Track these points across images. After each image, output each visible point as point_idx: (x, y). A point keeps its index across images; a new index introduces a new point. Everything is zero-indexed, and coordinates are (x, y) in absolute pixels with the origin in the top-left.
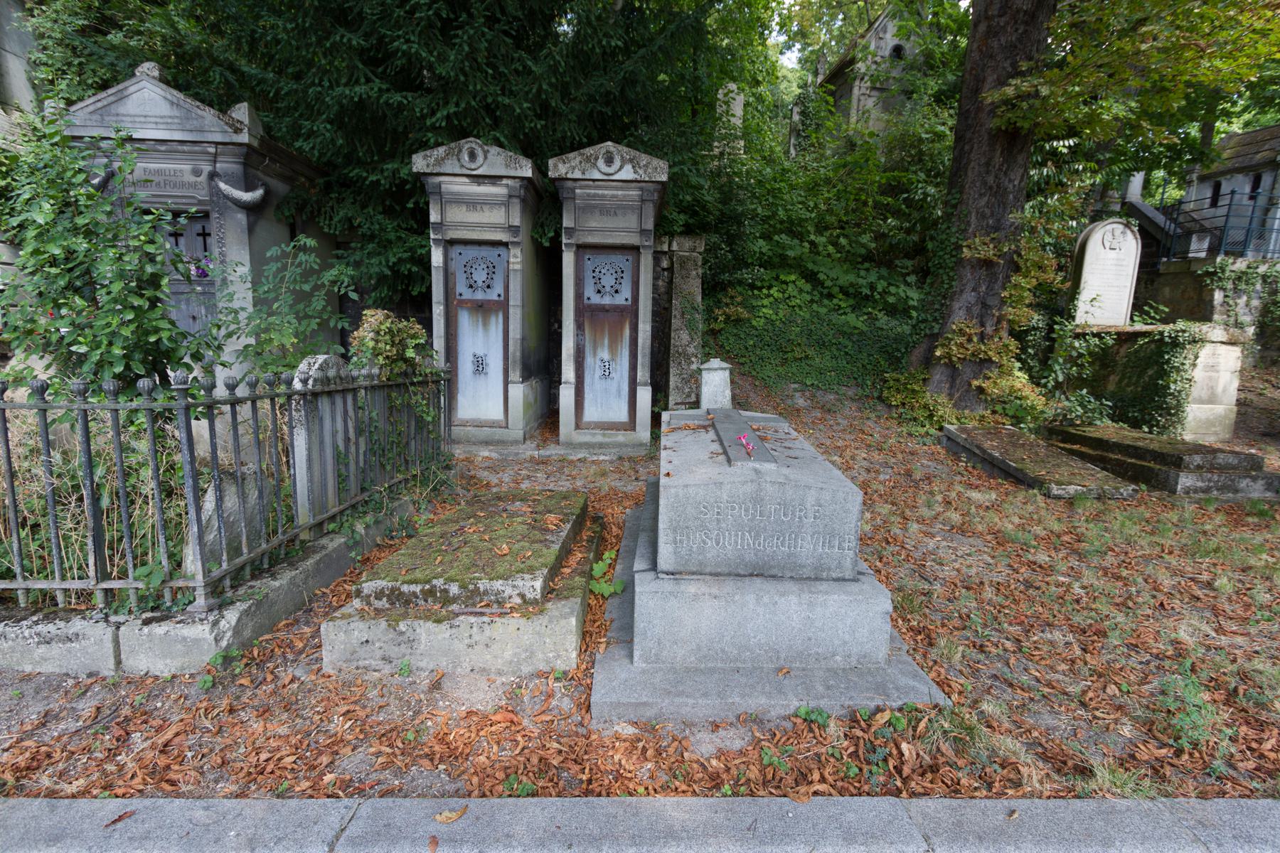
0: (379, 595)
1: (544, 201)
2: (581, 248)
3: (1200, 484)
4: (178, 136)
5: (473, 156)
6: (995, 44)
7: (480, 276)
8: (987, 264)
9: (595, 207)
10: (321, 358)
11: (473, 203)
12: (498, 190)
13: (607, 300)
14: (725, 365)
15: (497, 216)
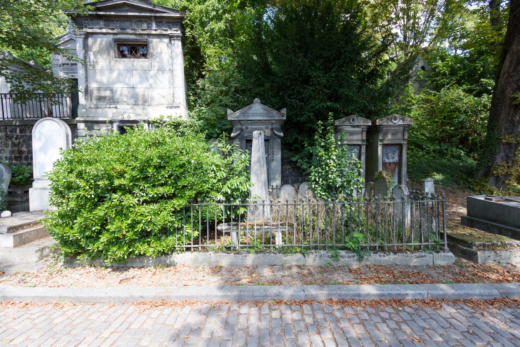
0: (480, 245)
2: (384, 145)
4: (265, 119)
5: (353, 120)
6: (511, 80)
8: (508, 144)
12: (359, 129)
13: (391, 161)
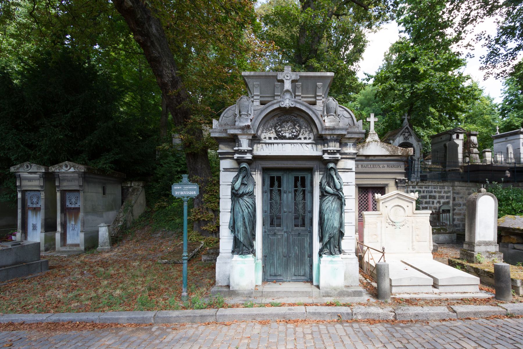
1: (49, 178)
3: (208, 258)
7: (35, 200)
9: (66, 179)
10: (405, 85)
11: (30, 180)
12: (37, 176)
13: (73, 206)
14: (105, 225)
15: (37, 183)
